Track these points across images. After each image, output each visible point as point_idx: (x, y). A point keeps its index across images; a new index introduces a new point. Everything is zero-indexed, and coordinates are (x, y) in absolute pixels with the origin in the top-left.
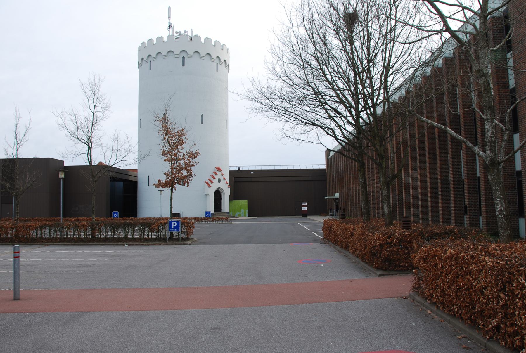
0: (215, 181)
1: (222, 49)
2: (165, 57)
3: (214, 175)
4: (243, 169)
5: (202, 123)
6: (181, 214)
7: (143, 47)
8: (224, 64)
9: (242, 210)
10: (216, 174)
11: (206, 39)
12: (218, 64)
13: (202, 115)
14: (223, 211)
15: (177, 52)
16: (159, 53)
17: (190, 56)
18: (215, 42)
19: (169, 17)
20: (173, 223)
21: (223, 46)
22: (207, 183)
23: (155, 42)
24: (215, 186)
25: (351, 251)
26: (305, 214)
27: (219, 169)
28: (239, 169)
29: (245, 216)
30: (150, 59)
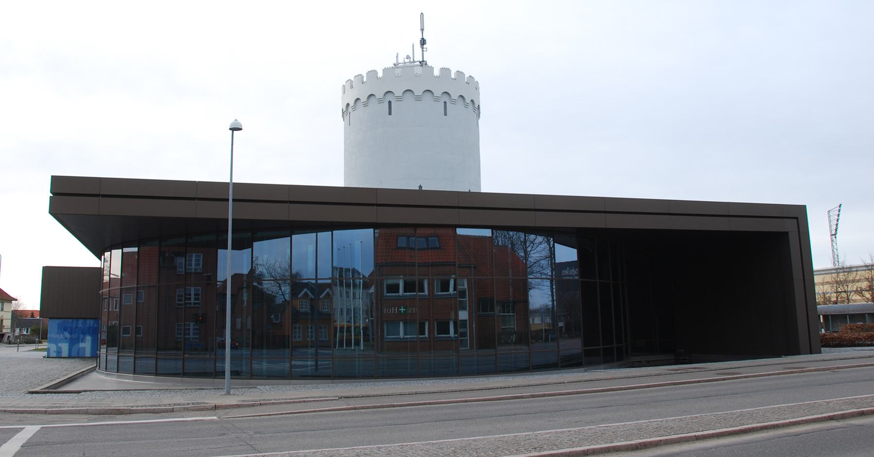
2: (365, 105)
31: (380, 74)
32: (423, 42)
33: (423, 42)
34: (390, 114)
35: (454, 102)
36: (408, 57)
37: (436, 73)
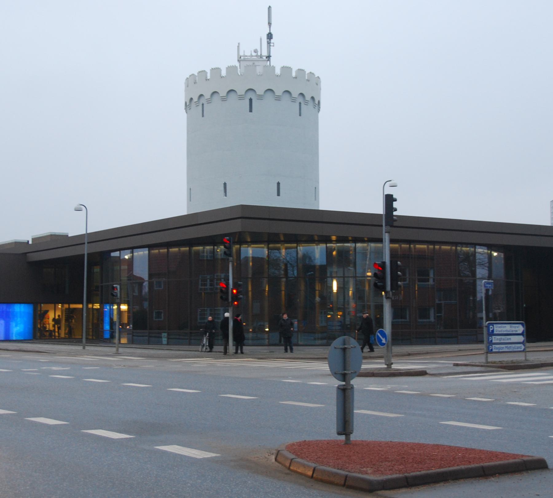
2: (224, 99)
7: (192, 81)
8: (311, 103)
16: (215, 92)
17: (260, 97)
25: (494, 459)
30: (203, 100)
31: (224, 73)
32: (270, 36)
33: (270, 36)
34: (251, 111)
35: (306, 103)
36: (256, 51)
37: (278, 71)
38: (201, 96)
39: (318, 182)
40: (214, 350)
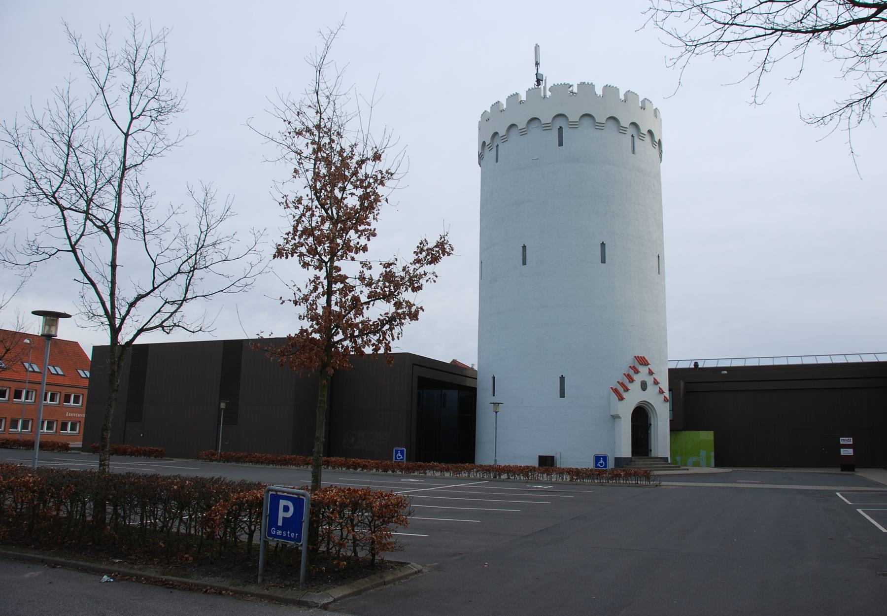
0: (635, 387)
1: (643, 108)
3: (631, 372)
4: (705, 366)
5: (603, 261)
6: (557, 457)
7: (486, 118)
8: (648, 138)
9: (703, 453)
10: (637, 372)
11: (607, 88)
12: (636, 139)
13: (603, 244)
14: (653, 454)
15: (546, 118)
17: (574, 125)
18: (625, 95)
19: (537, 64)
20: (282, 503)
21: (643, 102)
22: (616, 391)
23: (505, 107)
24: (634, 397)
26: (848, 465)
27: (643, 361)
28: (696, 364)
29: (708, 466)
30: (498, 141)
38: (496, 134)
39: (662, 245)
40: (693, 363)
